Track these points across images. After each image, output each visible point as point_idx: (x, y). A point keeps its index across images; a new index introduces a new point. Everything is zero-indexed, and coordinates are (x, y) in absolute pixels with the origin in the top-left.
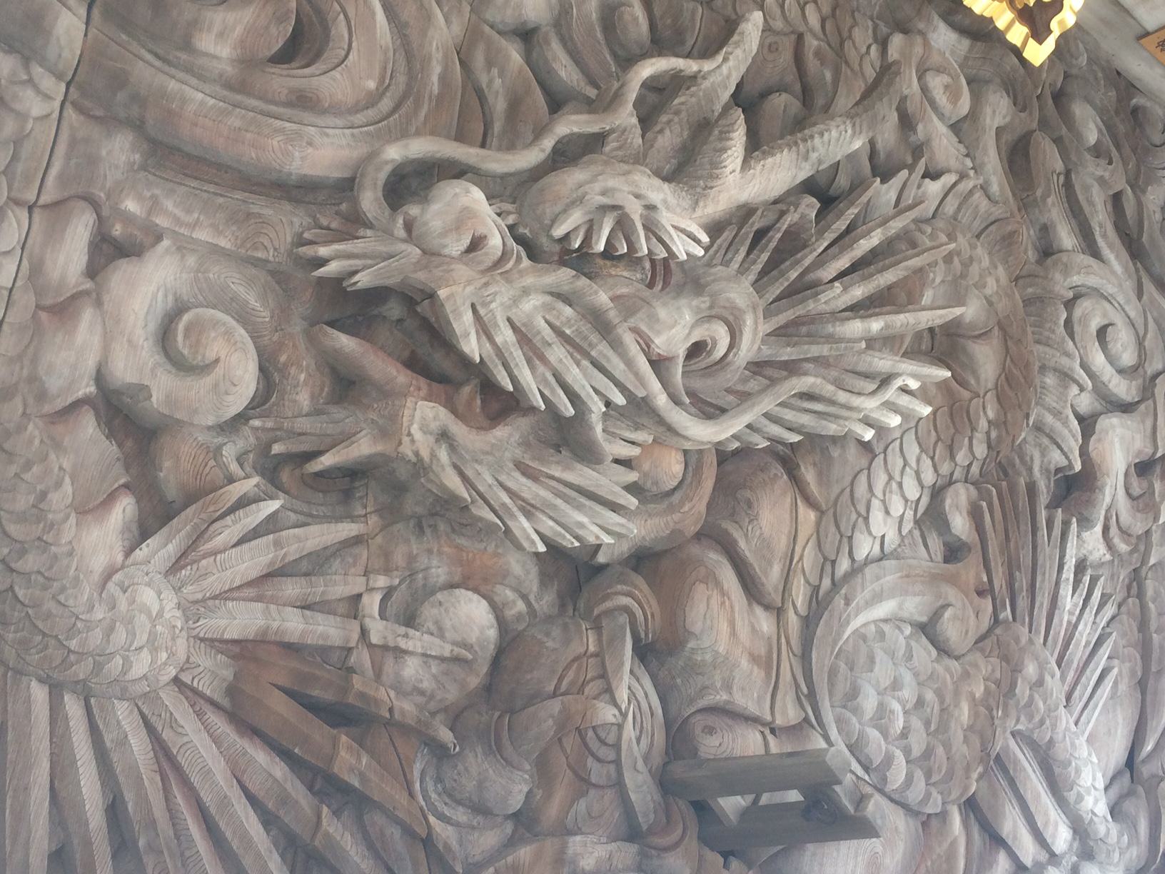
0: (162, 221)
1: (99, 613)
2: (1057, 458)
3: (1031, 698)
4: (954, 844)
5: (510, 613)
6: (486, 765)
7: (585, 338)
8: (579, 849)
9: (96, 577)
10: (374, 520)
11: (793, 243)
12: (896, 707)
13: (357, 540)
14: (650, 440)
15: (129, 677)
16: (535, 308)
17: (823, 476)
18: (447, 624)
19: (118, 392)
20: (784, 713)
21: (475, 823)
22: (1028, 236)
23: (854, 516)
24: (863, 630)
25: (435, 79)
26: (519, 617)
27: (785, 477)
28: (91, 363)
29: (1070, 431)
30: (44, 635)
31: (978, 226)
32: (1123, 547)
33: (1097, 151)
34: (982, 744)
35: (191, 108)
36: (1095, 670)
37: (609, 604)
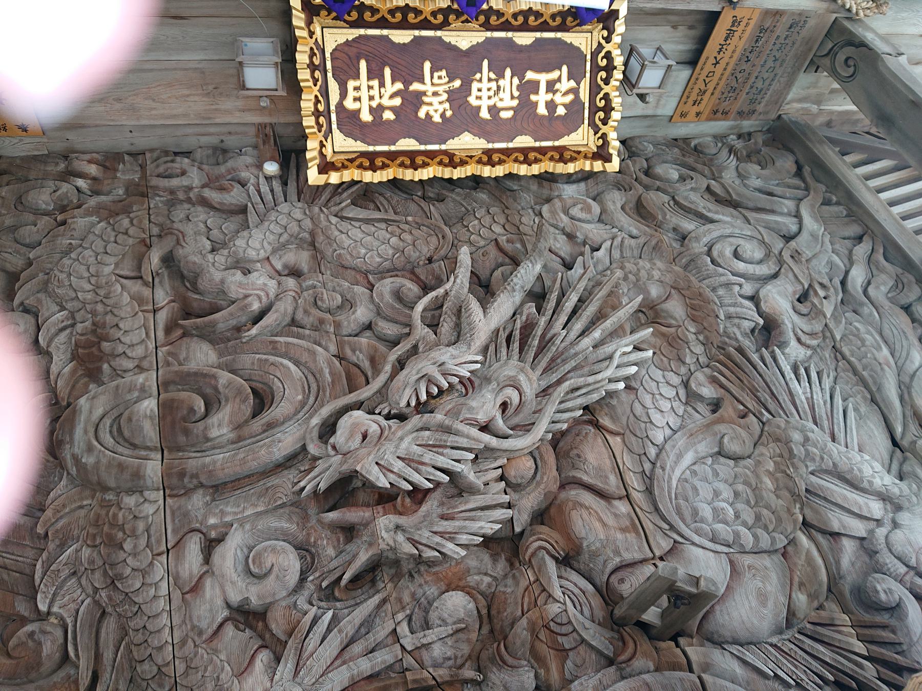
0: (228, 519)
2: (747, 325)
3: (806, 450)
4: (808, 552)
5: (483, 587)
7: (441, 440)
11: (528, 328)
12: (724, 505)
13: (384, 601)
16: (409, 443)
17: (614, 419)
18: (446, 616)
22: (668, 238)
23: (643, 425)
24: (683, 477)
25: (328, 375)
26: (489, 585)
28: (219, 602)
31: (636, 253)
32: (814, 342)
33: (682, 179)
34: (790, 492)
36: (838, 413)
37: (530, 551)
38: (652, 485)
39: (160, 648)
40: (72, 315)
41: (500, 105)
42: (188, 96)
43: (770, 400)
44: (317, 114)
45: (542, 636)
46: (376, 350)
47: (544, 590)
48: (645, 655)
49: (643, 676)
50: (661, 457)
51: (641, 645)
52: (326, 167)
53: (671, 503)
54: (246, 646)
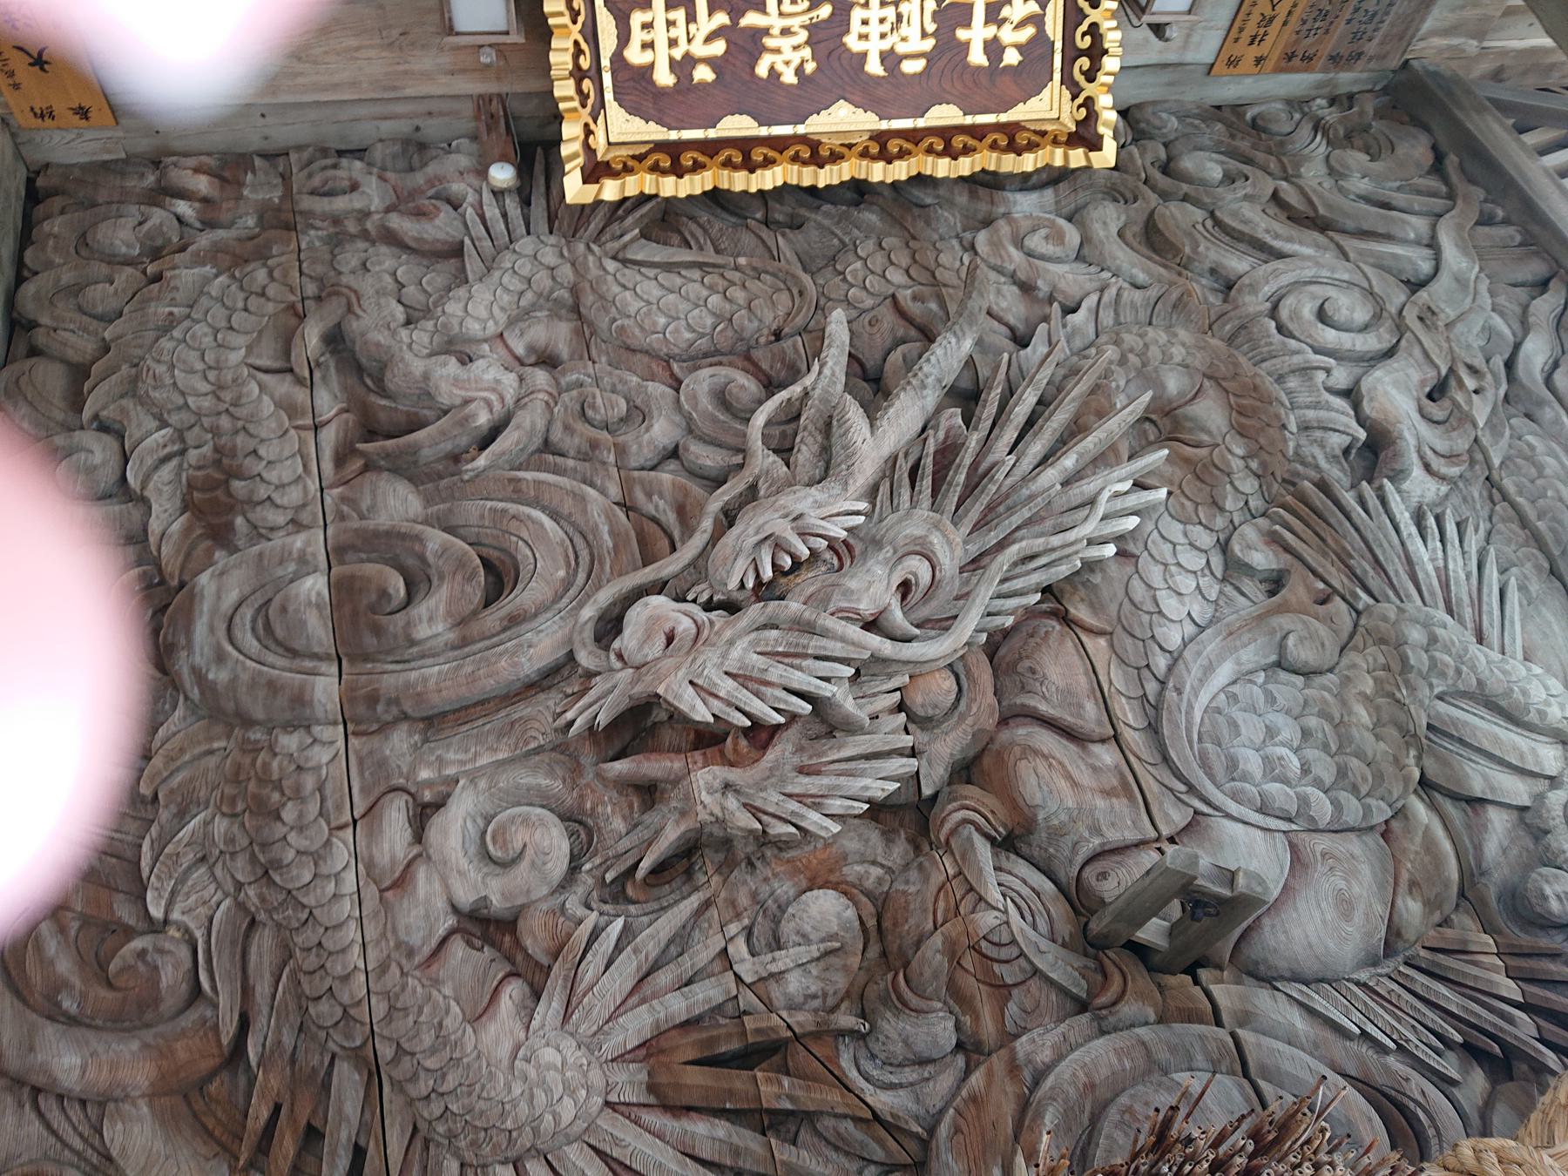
1: (517, 1090)
2: (1337, 441)
3: (1432, 658)
4: (1427, 830)
5: (869, 883)
6: (901, 1025)
8: (1029, 1048)
9: (506, 1063)
10: (716, 880)
11: (948, 454)
12: (1284, 751)
13: (707, 904)
14: (907, 679)
15: (563, 1125)
16: (745, 650)
17: (1096, 607)
18: (807, 928)
19: (472, 911)
20: (1169, 820)
21: (926, 1075)
23: (1146, 618)
24: (1214, 704)
25: (606, 537)
26: (880, 881)
27: (1058, 627)
28: (440, 904)
29: (1337, 411)
30: (486, 1130)
32: (1454, 471)
33: (1229, 179)
35: (432, 683)
37: (948, 826)
38: (1158, 718)
39: (345, 978)
40: (180, 435)
41: (901, 49)
42: (358, 49)
43: (1371, 572)
44: (578, 74)
45: (968, 962)
46: (686, 492)
47: (971, 889)
48: (1142, 996)
49: (1138, 1030)
50: (1176, 671)
51: (1134, 980)
52: (595, 171)
53: (1191, 748)
54: (485, 974)
